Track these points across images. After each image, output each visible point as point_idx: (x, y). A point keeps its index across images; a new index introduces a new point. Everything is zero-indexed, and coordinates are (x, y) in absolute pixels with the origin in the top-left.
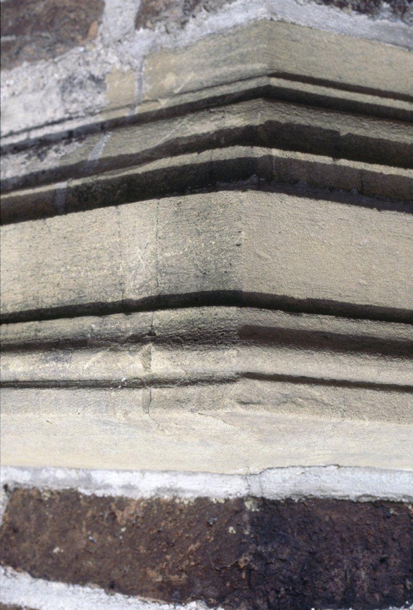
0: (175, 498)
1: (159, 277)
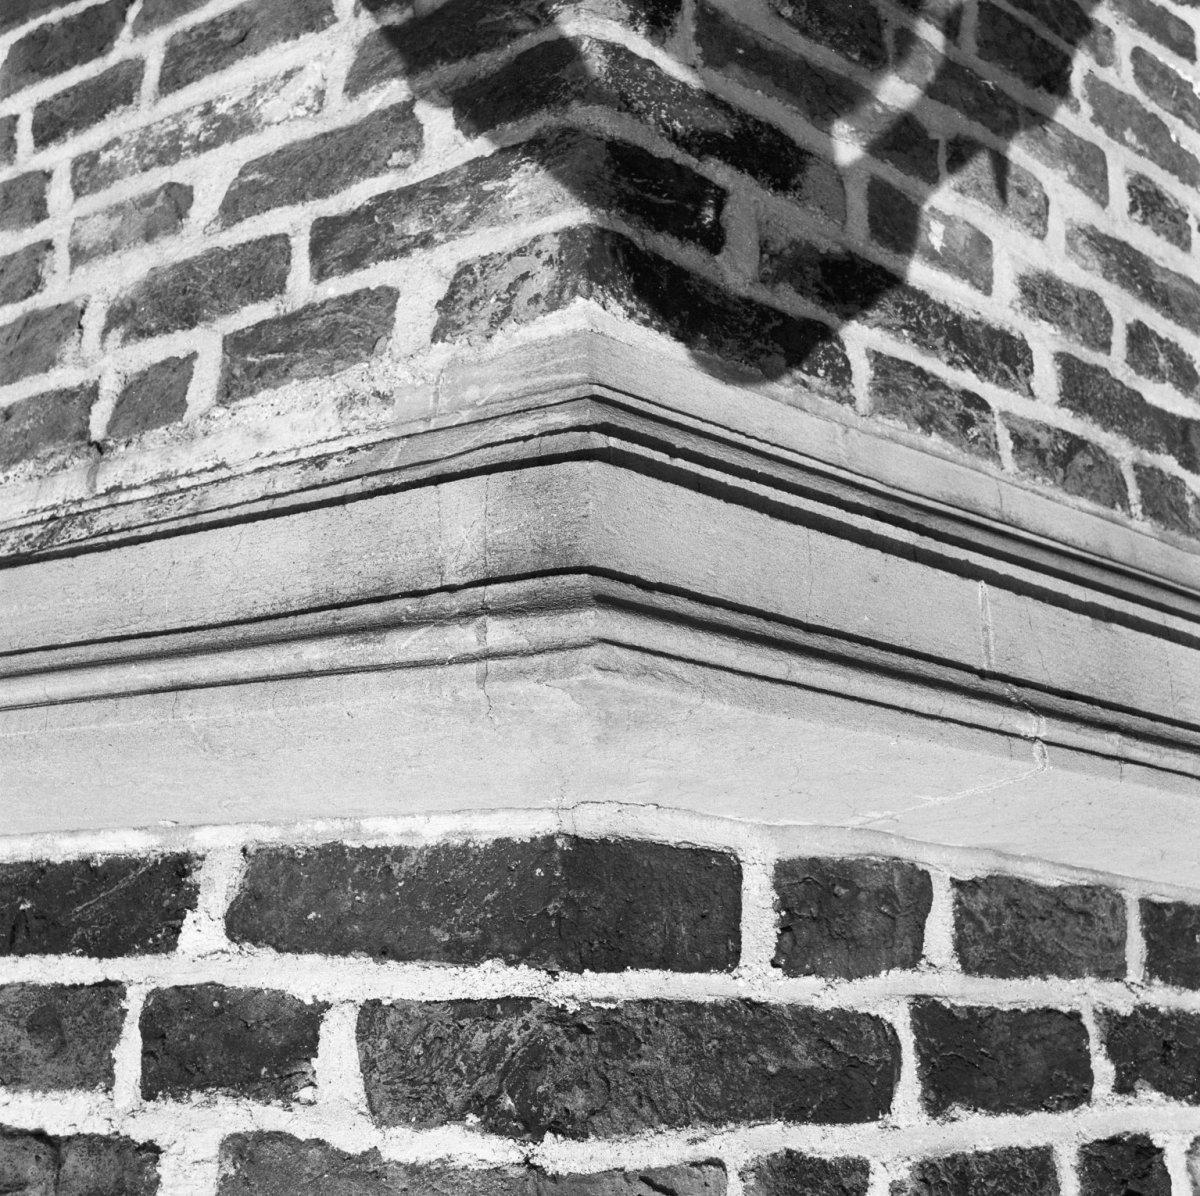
0: (468, 842)
1: (487, 556)
